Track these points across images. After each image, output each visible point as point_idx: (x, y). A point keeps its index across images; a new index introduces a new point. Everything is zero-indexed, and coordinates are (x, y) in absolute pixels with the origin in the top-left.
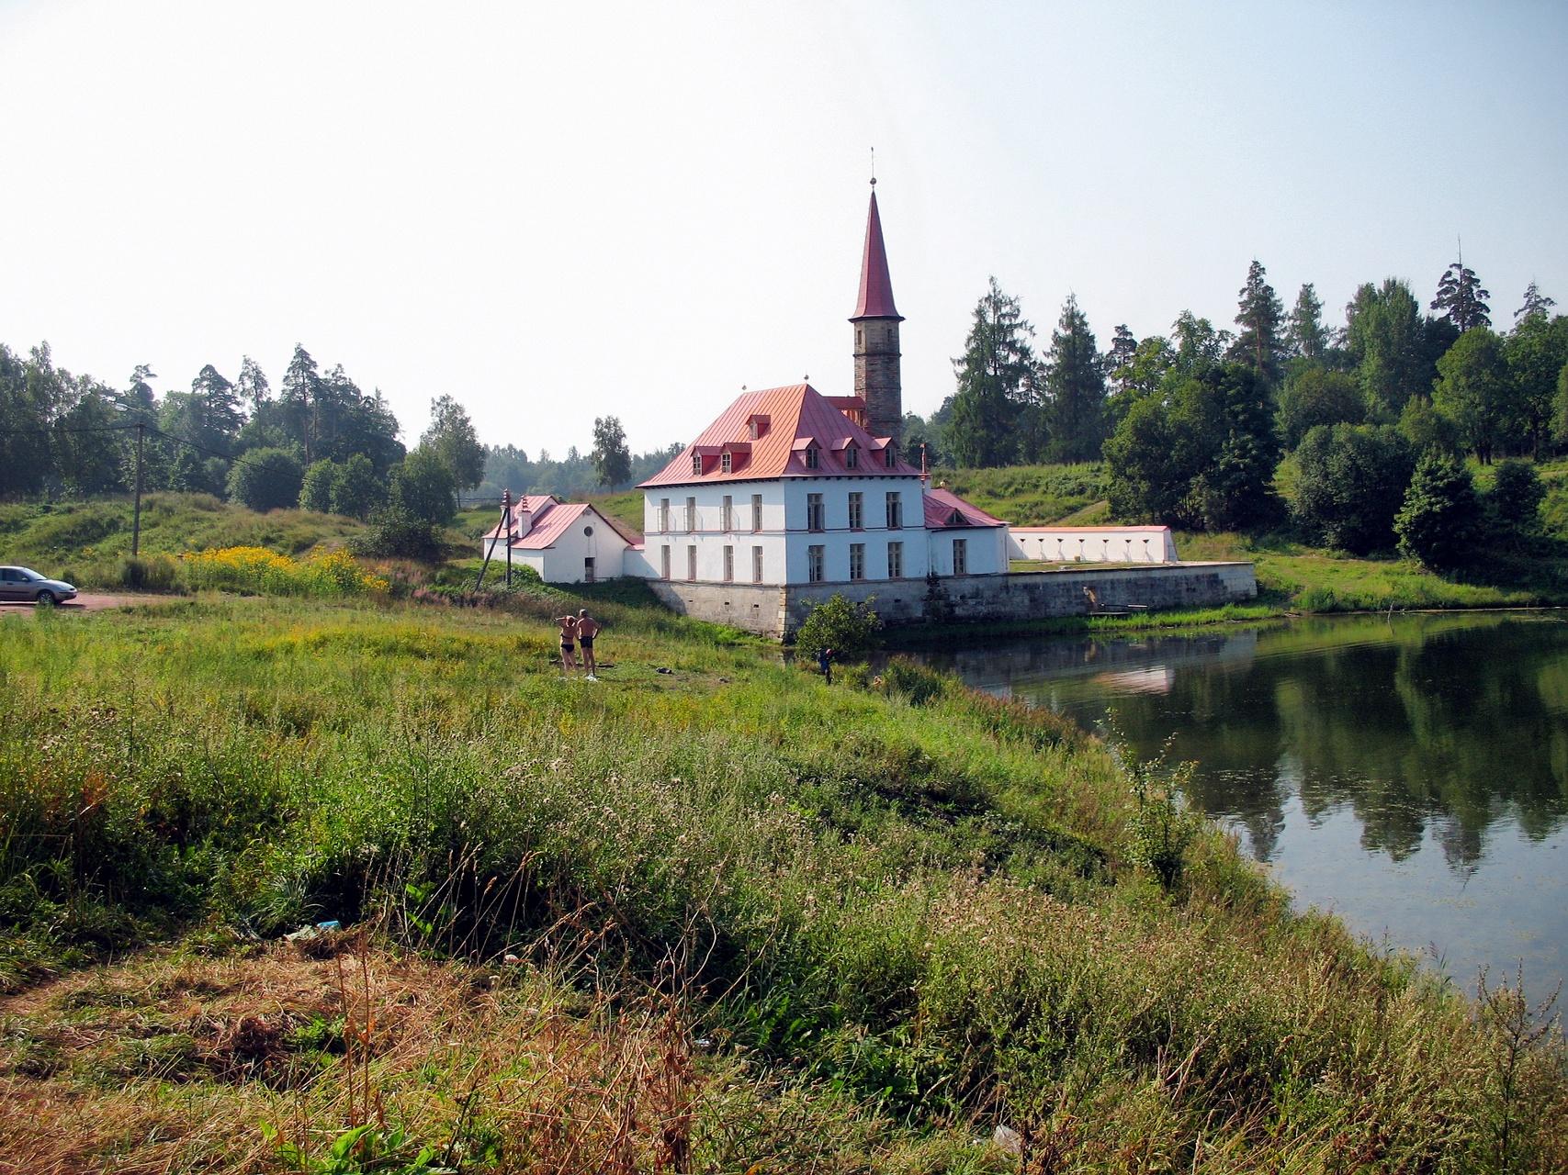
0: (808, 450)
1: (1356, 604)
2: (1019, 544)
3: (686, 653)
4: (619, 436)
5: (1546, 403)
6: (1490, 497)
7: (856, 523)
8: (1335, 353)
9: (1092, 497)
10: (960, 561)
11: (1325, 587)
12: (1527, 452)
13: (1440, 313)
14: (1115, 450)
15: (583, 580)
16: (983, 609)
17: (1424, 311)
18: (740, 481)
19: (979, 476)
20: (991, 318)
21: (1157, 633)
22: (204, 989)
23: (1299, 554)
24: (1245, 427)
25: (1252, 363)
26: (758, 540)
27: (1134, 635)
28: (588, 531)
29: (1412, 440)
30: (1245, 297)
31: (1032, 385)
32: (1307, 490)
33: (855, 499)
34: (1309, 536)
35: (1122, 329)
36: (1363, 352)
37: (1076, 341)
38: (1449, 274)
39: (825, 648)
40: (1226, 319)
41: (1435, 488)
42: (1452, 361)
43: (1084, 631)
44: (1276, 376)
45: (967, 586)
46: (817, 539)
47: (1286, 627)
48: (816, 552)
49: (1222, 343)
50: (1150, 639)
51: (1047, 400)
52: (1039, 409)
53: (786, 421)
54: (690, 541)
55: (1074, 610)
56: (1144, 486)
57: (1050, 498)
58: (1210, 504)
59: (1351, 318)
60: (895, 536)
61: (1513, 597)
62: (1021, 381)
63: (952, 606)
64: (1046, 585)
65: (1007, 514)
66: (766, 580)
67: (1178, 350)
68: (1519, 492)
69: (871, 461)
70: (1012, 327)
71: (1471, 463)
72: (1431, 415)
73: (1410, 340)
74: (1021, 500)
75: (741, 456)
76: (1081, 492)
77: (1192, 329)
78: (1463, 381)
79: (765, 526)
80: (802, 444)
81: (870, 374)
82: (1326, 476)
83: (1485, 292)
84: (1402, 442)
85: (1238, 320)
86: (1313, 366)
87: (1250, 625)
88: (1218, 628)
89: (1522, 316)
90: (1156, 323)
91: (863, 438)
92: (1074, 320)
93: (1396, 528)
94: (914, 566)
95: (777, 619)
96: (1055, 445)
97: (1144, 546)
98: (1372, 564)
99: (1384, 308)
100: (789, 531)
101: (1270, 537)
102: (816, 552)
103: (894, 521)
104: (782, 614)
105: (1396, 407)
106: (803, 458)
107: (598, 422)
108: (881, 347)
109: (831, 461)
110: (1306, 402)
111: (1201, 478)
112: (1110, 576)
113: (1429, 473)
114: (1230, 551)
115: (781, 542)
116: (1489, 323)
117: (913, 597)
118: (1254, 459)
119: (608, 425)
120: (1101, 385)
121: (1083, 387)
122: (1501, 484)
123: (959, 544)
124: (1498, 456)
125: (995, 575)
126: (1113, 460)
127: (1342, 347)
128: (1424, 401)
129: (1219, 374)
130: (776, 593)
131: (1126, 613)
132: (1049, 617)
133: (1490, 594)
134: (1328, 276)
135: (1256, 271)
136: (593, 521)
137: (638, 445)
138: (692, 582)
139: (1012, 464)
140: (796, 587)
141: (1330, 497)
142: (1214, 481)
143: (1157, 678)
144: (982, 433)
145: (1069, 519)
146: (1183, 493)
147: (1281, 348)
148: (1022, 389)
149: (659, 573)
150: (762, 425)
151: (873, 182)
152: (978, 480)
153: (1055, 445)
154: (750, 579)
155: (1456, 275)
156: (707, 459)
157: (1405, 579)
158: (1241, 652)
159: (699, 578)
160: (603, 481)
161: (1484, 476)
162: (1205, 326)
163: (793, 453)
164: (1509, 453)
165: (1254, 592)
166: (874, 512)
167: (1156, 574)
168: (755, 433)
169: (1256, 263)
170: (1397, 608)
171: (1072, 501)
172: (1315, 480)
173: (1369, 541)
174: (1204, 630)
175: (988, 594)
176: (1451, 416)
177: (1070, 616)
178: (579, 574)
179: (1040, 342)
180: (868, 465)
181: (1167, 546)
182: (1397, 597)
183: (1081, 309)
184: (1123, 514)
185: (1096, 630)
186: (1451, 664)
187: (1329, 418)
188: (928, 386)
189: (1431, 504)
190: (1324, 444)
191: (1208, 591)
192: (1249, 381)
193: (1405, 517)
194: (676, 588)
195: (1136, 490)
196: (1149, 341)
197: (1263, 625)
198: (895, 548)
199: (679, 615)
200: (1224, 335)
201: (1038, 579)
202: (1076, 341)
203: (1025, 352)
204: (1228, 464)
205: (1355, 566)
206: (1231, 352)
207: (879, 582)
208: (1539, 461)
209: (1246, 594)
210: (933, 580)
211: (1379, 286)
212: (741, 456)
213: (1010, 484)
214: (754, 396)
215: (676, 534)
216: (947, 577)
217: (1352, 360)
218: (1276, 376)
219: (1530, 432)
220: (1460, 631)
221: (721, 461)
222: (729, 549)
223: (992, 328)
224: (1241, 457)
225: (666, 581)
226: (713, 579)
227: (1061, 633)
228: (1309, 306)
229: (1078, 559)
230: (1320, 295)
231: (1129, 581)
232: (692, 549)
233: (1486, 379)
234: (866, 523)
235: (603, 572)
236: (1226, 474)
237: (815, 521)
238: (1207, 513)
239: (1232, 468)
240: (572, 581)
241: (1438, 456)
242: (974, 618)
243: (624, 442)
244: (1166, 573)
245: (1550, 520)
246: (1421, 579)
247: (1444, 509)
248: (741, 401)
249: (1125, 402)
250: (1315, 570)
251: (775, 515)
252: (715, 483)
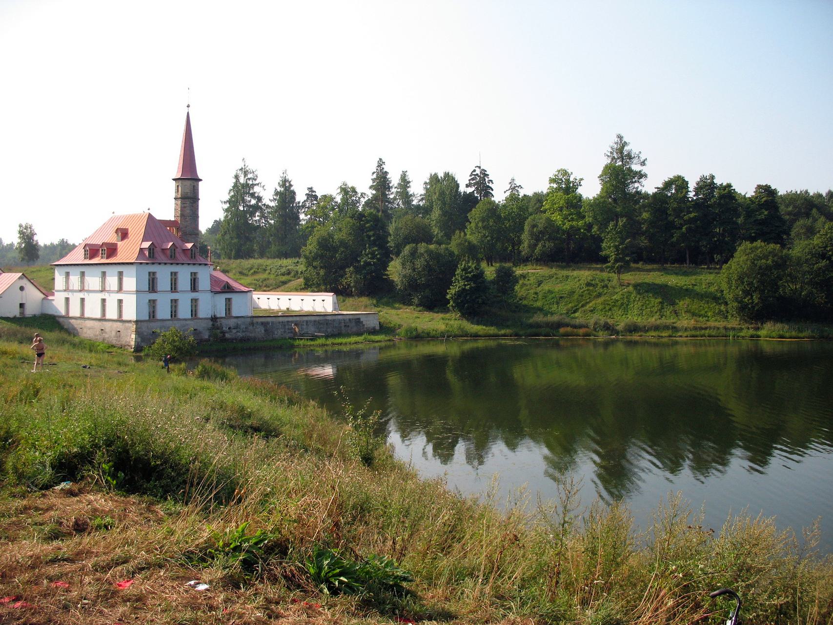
0: (149, 248)
1: (428, 334)
2: (257, 300)
3: (86, 358)
4: (33, 234)
5: (518, 237)
6: (493, 282)
7: (174, 288)
8: (418, 207)
9: (294, 276)
10: (228, 309)
11: (413, 325)
12: (509, 261)
13: (470, 190)
14: (307, 253)
15: (18, 315)
16: (240, 335)
17: (462, 189)
18: (111, 264)
19: (235, 264)
20: (242, 180)
21: (329, 348)
22: (37, 509)
23: (400, 309)
24: (374, 244)
25: (378, 211)
26: (120, 296)
27: (318, 349)
28: (22, 288)
29: (456, 253)
30: (375, 176)
31: (262, 216)
32: (405, 276)
33: (174, 275)
34: (406, 301)
36: (432, 207)
37: (286, 194)
38: (474, 171)
39: (166, 355)
40: (365, 188)
41: (467, 277)
42: (475, 214)
43: (292, 346)
44: (389, 217)
45: (232, 322)
46: (153, 296)
47: (394, 345)
48: (153, 303)
49: (362, 199)
50: (326, 351)
51: (270, 224)
52: (268, 231)
53: (137, 232)
54: (81, 295)
55: (288, 336)
56: (322, 272)
57: (272, 277)
58: (356, 282)
59: (427, 189)
60: (194, 295)
61: (503, 332)
62: (257, 214)
63: (224, 333)
64: (272, 323)
65: (250, 284)
66: (125, 318)
67: (339, 201)
68: (506, 280)
69: (182, 255)
70: (253, 185)
71: (484, 265)
72: (466, 241)
73: (455, 203)
74: (257, 277)
75: (111, 250)
76: (289, 274)
77: (347, 192)
78: (480, 224)
80: (146, 245)
81: (183, 209)
82: (414, 270)
84: (451, 254)
85: (371, 187)
86: (406, 213)
87: (377, 345)
88: (360, 346)
89: (508, 193)
90: (329, 187)
91: (179, 243)
92: (286, 184)
93: (448, 297)
94: (204, 312)
95: (131, 339)
96: (274, 248)
97: (322, 303)
98: (436, 315)
99: (442, 187)
100: (138, 292)
101: (385, 299)
102: (153, 303)
103: (194, 287)
104: (133, 336)
105: (448, 236)
106: (147, 253)
107: (20, 226)
108: (189, 195)
109: (161, 254)
110: (403, 232)
111: (351, 268)
112: (305, 319)
113: (464, 270)
114: (366, 307)
115: (134, 297)
117: (204, 327)
118: (378, 259)
119: (26, 228)
120: (298, 218)
121: (290, 219)
122: (498, 276)
123: (228, 301)
124: (496, 262)
125: (248, 317)
126: (306, 257)
127: (421, 204)
128: (462, 234)
129: (361, 215)
130: (130, 325)
131: (314, 338)
132: (274, 339)
133: (492, 330)
134: (416, 170)
135: (381, 163)
136: (25, 283)
137: (43, 239)
138: (82, 317)
139: (252, 257)
140: (141, 321)
141: (416, 280)
142: (358, 270)
143: (328, 371)
144: (235, 241)
145: (282, 288)
146: (342, 276)
147: (390, 203)
148: (257, 218)
149: (63, 313)
150: (123, 234)
151: (188, 106)
152: (234, 266)
153: (274, 248)
154: (115, 317)
155: (478, 171)
156: (92, 251)
157: (452, 322)
158: (371, 357)
159: (87, 315)
160: (23, 259)
161: (490, 272)
162: (354, 190)
163: (141, 249)
164: (501, 261)
165: (378, 328)
166: (184, 282)
167: (329, 318)
168: (120, 238)
170: (448, 337)
171: (284, 278)
172: (408, 271)
173: (434, 303)
174: (353, 346)
175: (243, 326)
176: (475, 242)
177: (285, 339)
178: (15, 312)
179: (268, 195)
180: (181, 258)
181: (334, 303)
182: (448, 331)
183: (289, 178)
184: (310, 286)
185: (298, 346)
186: (473, 364)
187: (416, 240)
188: (211, 211)
189: (465, 285)
190: (413, 254)
191: (355, 326)
192: (376, 219)
193: (452, 291)
194: (72, 321)
195: (318, 274)
196: (325, 196)
197: (383, 344)
198: (194, 301)
199: (74, 336)
200: (363, 195)
201: (269, 320)
202: (286, 194)
203: (259, 199)
204: (365, 262)
205: (428, 315)
206: (367, 203)
207: (186, 320)
208: (515, 265)
209: (374, 328)
210: (214, 319)
211: (441, 175)
212: (111, 250)
213: (251, 269)
214: (119, 218)
215: (73, 291)
217: (426, 210)
218: (389, 217)
219: (511, 251)
220: (477, 348)
221: (101, 253)
222: (104, 301)
223: (243, 185)
224: (372, 258)
227: (281, 348)
228: (405, 182)
229: (288, 309)
230: (410, 177)
231: (315, 321)
232: (83, 300)
233: (491, 224)
235: (29, 311)
236: (364, 267)
237: (152, 287)
238: (354, 286)
239: (367, 264)
240: (11, 315)
241: (469, 262)
242: (236, 339)
243: (35, 238)
244: (334, 317)
245: (520, 295)
246: (460, 322)
247: (471, 288)
248: (112, 220)
249: (311, 227)
250: (407, 317)
251: (130, 283)
252: (96, 264)
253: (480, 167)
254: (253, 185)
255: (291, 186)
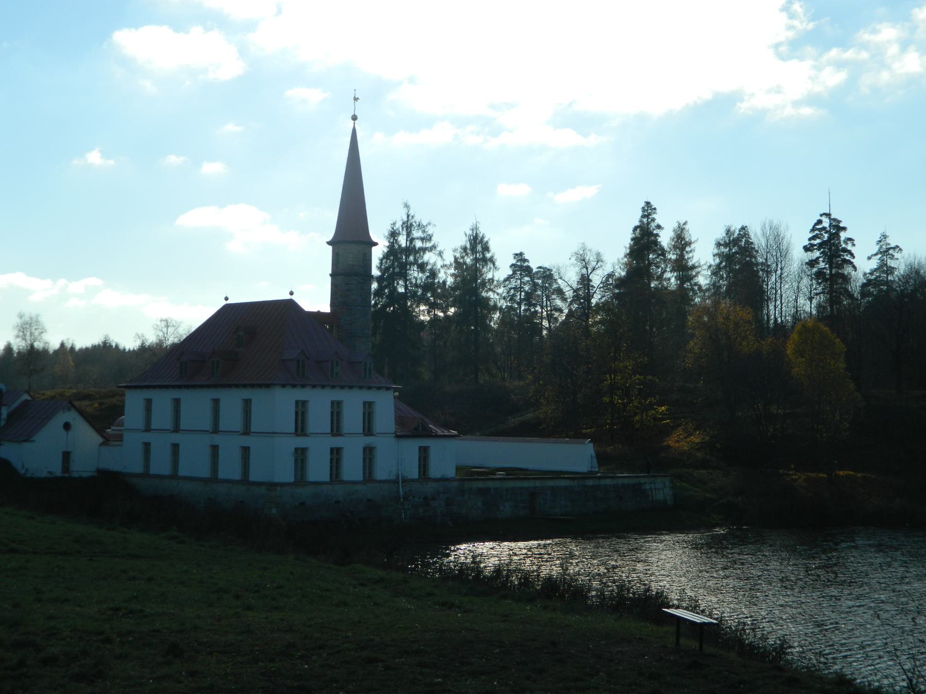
7: (336, 429)
33: (337, 407)
35: (520, 256)
38: (820, 222)
40: (614, 256)
70: (424, 250)
79: (153, 427)
83: (850, 239)
92: (477, 244)
116: (855, 268)
135: (648, 210)
138: (245, 480)
151: (354, 118)
154: (237, 475)
166: (352, 419)
169: (648, 203)
198: (369, 452)
203: (433, 274)
216: (413, 480)
225: (146, 475)
226: (353, 479)
228: (681, 242)
230: (692, 233)
234: (311, 427)
240: (439, 476)
253: (828, 215)
254: (424, 250)
255: (486, 248)
